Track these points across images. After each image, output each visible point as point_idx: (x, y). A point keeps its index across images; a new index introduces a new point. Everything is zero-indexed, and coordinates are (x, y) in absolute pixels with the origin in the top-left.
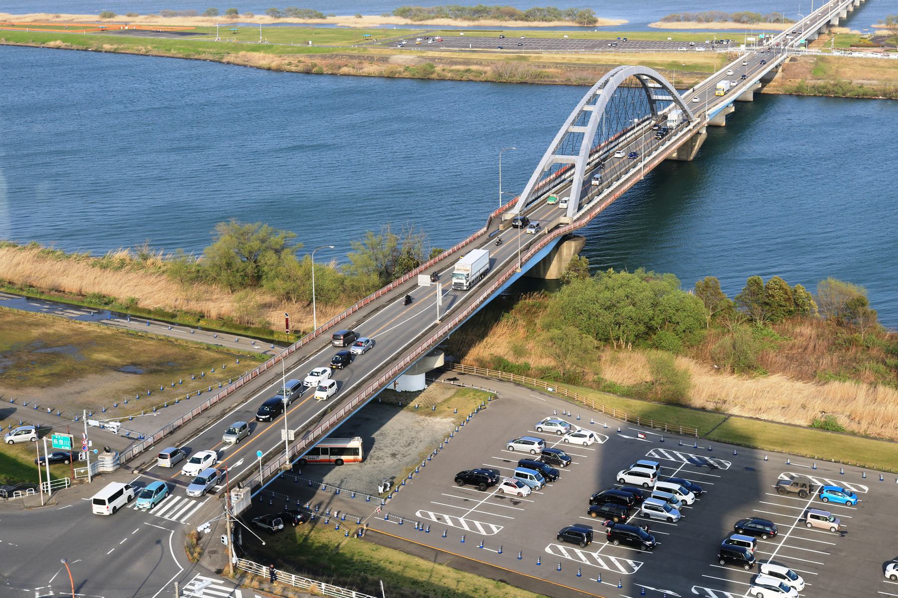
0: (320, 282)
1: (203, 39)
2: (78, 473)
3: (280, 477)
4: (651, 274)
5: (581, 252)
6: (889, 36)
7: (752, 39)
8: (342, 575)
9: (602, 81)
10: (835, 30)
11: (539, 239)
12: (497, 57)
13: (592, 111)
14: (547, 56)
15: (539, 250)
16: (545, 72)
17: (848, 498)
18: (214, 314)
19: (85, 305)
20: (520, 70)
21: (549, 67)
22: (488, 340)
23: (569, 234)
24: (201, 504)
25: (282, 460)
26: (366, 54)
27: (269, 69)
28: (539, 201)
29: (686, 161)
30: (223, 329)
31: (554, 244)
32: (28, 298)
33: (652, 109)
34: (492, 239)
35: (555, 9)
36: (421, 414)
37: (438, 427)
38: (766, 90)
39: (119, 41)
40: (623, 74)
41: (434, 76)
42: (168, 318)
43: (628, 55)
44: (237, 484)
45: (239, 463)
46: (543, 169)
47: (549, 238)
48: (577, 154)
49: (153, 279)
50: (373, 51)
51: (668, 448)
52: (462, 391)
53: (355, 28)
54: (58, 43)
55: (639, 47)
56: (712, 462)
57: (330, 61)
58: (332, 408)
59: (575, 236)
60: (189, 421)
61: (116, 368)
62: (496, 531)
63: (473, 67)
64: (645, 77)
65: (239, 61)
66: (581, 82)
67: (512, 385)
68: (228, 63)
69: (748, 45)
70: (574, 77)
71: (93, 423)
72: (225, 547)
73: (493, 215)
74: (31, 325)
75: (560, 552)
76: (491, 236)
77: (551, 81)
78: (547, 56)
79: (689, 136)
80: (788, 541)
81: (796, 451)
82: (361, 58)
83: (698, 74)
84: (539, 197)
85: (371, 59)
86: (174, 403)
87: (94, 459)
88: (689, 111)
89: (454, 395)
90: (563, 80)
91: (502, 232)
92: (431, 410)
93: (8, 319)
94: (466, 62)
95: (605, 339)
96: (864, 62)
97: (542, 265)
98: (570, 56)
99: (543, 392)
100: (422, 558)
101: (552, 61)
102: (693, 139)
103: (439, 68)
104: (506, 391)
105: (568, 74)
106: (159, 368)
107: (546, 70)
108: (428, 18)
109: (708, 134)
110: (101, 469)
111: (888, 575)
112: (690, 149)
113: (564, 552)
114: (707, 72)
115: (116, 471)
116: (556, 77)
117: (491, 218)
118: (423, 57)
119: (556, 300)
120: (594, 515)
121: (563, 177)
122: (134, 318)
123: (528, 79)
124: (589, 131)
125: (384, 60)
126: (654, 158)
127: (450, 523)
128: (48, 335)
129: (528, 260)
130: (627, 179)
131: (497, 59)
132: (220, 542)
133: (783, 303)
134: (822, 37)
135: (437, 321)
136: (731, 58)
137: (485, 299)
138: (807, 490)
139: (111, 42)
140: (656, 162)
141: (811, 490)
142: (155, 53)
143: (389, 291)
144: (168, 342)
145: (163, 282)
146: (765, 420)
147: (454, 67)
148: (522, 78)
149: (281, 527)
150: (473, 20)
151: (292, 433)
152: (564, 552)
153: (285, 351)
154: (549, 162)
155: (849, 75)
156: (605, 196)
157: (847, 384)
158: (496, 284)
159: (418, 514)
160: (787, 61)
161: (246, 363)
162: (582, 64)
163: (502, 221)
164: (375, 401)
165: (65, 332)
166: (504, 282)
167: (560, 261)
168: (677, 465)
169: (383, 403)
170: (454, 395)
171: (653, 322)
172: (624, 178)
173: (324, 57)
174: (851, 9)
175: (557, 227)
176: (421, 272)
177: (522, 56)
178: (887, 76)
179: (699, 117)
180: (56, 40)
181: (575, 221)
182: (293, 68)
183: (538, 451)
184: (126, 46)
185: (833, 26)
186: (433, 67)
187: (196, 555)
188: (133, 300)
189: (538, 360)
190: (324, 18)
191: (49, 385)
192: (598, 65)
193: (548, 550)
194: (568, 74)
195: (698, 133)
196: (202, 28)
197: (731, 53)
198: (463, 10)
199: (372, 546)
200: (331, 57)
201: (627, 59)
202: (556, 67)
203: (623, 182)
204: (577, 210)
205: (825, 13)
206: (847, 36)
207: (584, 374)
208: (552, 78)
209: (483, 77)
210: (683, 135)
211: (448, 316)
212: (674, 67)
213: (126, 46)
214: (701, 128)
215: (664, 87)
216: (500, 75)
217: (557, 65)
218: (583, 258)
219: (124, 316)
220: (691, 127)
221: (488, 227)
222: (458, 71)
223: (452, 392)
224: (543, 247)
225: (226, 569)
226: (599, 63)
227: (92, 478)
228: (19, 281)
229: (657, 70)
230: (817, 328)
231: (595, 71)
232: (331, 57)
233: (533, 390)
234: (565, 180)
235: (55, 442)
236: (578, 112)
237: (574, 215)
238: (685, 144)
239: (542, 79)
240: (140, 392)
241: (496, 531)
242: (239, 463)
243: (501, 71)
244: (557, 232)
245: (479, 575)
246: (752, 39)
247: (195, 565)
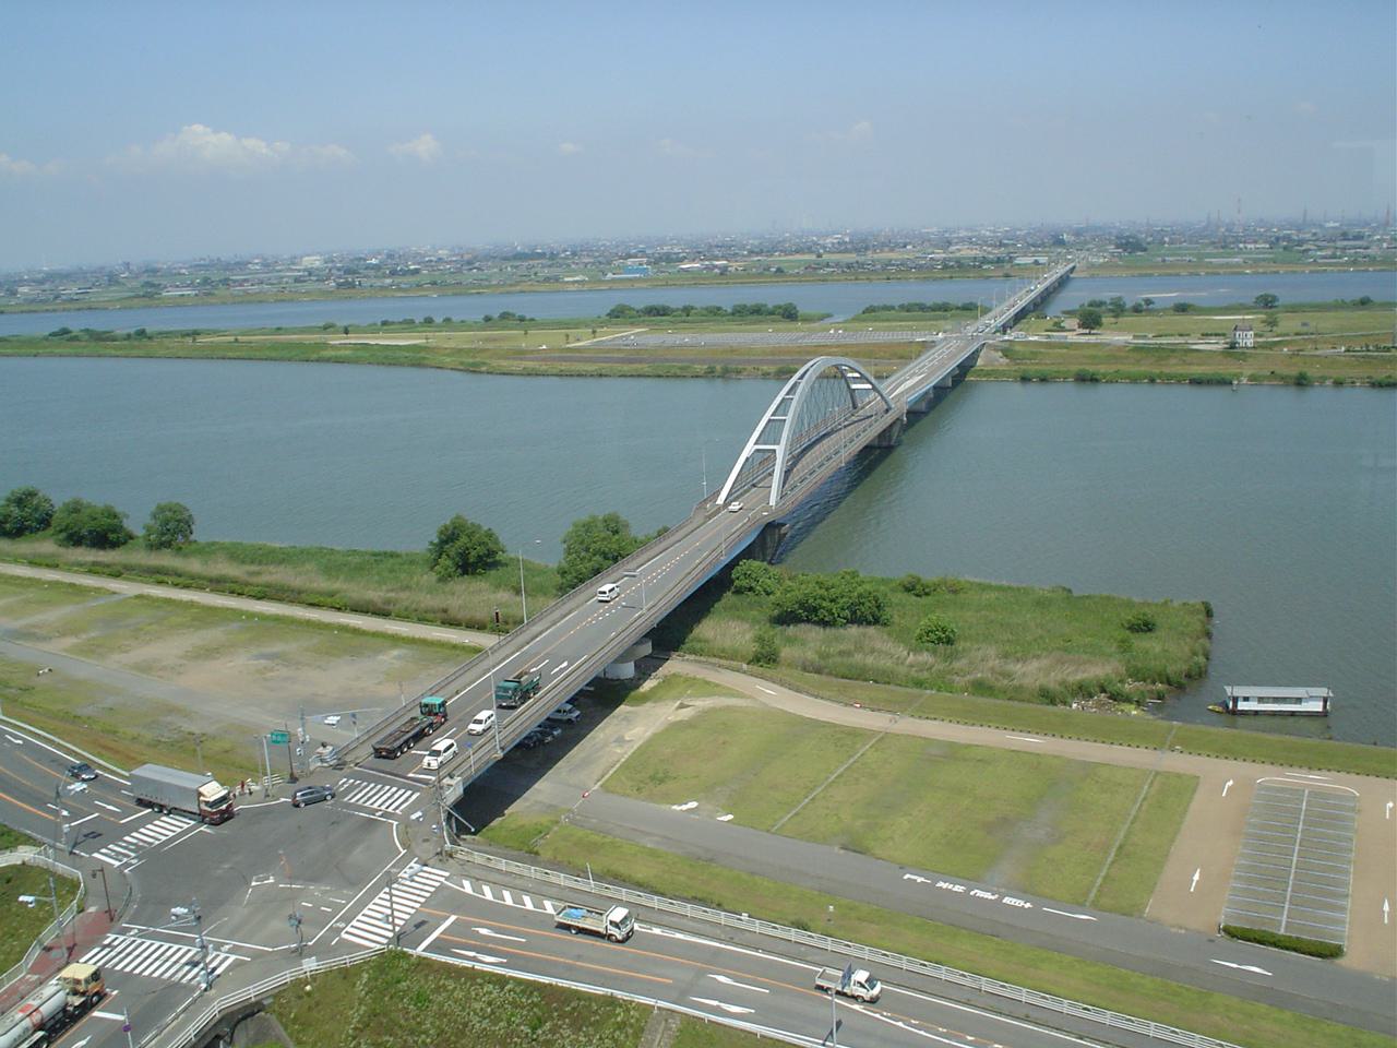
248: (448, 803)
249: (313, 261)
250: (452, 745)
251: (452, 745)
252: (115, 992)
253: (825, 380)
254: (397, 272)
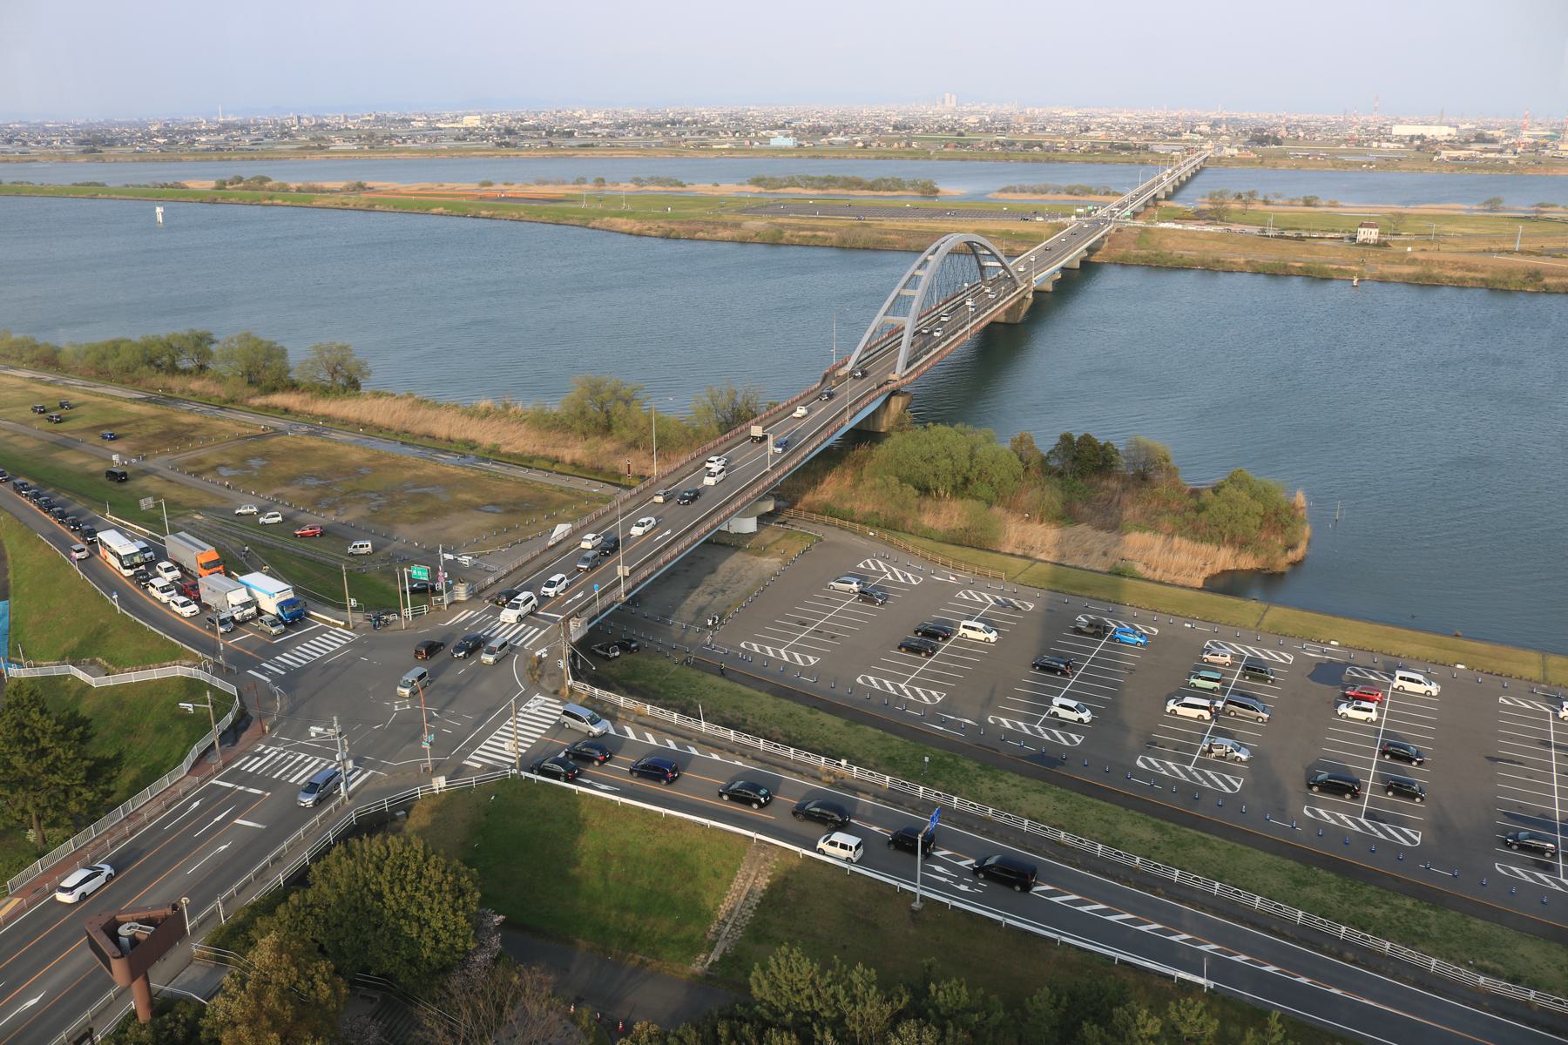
0: (660, 431)
1: (572, 206)
2: (436, 602)
3: (618, 608)
5: (905, 408)
6: (1211, 210)
7: (1080, 210)
8: (670, 698)
9: (933, 247)
10: (1161, 203)
14: (889, 223)
17: (1138, 639)
18: (568, 459)
19: (453, 449)
21: (890, 234)
22: (820, 488)
24: (543, 632)
25: (618, 594)
26: (720, 220)
27: (630, 234)
30: (575, 473)
31: (882, 399)
32: (403, 443)
33: (982, 275)
35: (899, 180)
36: (752, 554)
37: (766, 566)
38: (1094, 259)
39: (495, 208)
40: (954, 240)
41: (783, 241)
42: (526, 461)
44: (574, 615)
45: (579, 595)
48: (907, 316)
49: (514, 427)
50: (727, 217)
51: (978, 590)
52: (789, 535)
53: (713, 196)
54: (441, 209)
55: (977, 216)
56: (1016, 603)
57: (687, 227)
58: (667, 547)
60: (536, 556)
61: (477, 507)
62: (813, 662)
63: (820, 233)
65: (603, 226)
67: (836, 529)
68: (594, 228)
69: (1078, 215)
70: (913, 243)
71: (449, 557)
72: (562, 671)
74: (403, 467)
75: (870, 683)
78: (889, 223)
80: (1081, 677)
81: (1094, 595)
82: (716, 224)
85: (725, 225)
86: (528, 540)
87: (449, 588)
89: (782, 538)
91: (834, 387)
92: (761, 551)
93: (384, 462)
94: (814, 229)
95: (925, 490)
96: (1185, 234)
98: (910, 224)
99: (864, 536)
100: (744, 685)
102: (1020, 303)
103: (788, 233)
104: (832, 535)
105: (908, 240)
106: (516, 508)
108: (781, 187)
110: (456, 598)
111: (1168, 710)
113: (874, 682)
115: (469, 600)
118: (774, 224)
119: (882, 451)
120: (903, 650)
122: (496, 461)
123: (870, 245)
124: (918, 294)
125: (737, 225)
127: (771, 654)
128: (419, 476)
132: (556, 666)
133: (1092, 458)
134: (1149, 209)
135: (768, 469)
136: (1061, 227)
137: (814, 449)
138: (1102, 631)
139: (488, 208)
140: (983, 324)
141: (1105, 631)
142: (527, 218)
143: (726, 440)
144: (524, 483)
145: (523, 429)
146: (1068, 566)
147: (801, 233)
149: (617, 654)
150: (823, 189)
151: (627, 569)
152: (874, 682)
153: (626, 494)
155: (1171, 245)
157: (1147, 534)
159: (742, 645)
160: (1113, 232)
161: (594, 505)
164: (707, 542)
165: (433, 474)
168: (984, 605)
169: (716, 543)
170: (782, 538)
171: (970, 473)
173: (682, 223)
174: (1177, 183)
176: (756, 424)
178: (1206, 248)
180: (439, 207)
182: (653, 233)
183: (856, 590)
184: (501, 212)
185: (1160, 199)
186: (781, 232)
187: (536, 677)
188: (495, 445)
189: (865, 505)
190: (684, 186)
191: (417, 521)
193: (859, 680)
194: (908, 240)
195: (1024, 298)
196: (571, 195)
197: (1061, 223)
198: (812, 179)
199: (700, 673)
200: (689, 222)
205: (1152, 186)
206: (1172, 209)
207: (904, 520)
209: (828, 243)
211: (778, 464)
212: (1007, 235)
213: (501, 212)
215: (993, 254)
216: (844, 241)
217: (897, 232)
219: (487, 460)
220: (1019, 290)
222: (805, 236)
223: (780, 535)
224: (871, 402)
225: (562, 691)
227: (448, 606)
228: (396, 428)
229: (988, 238)
230: (1123, 482)
232: (689, 222)
233: (855, 533)
235: (414, 572)
238: (1012, 307)
240: (499, 530)
241: (813, 662)
242: (579, 595)
244: (885, 387)
245: (795, 702)
246: (1080, 210)
247: (535, 686)
248: (573, 641)
249: (472, 121)
250: (531, 598)
251: (531, 598)
252: (268, 794)
253: (956, 257)
254: (556, 136)
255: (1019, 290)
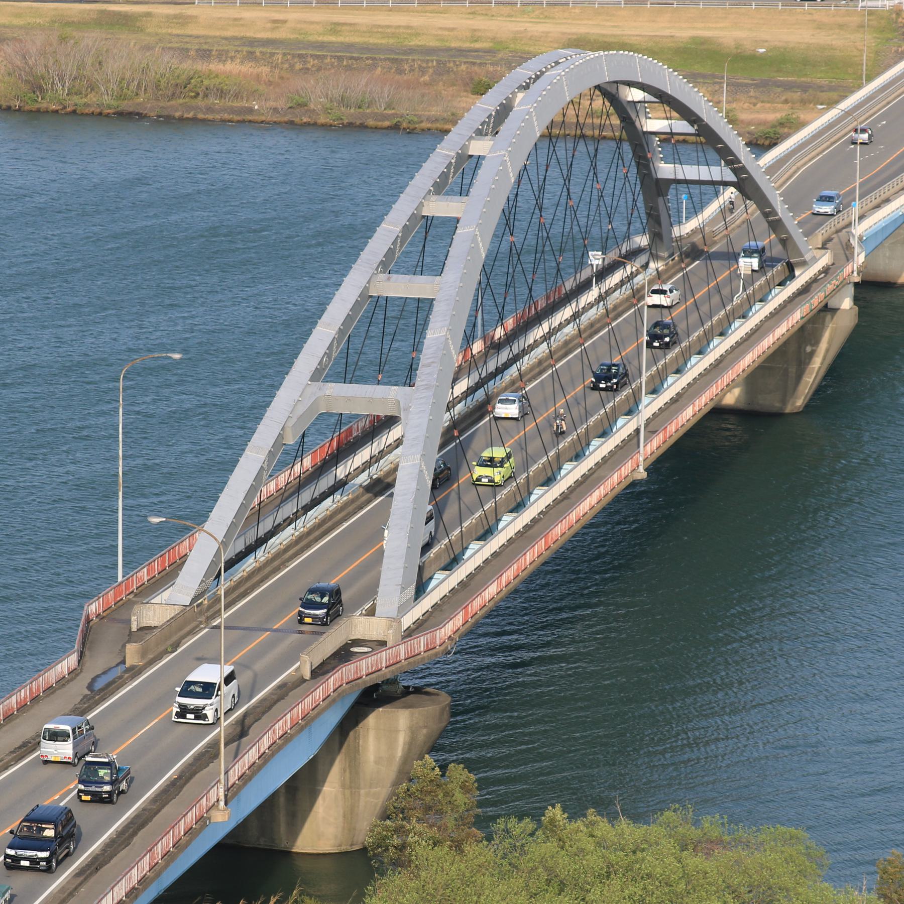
4: (712, 825)
11: (281, 698)
12: (18, 15)
13: (458, 220)
15: (286, 738)
16: (210, 75)
20: (113, 67)
21: (222, 56)
23: (388, 682)
28: (261, 555)
29: (777, 416)
31: (333, 718)
34: (103, 699)
43: (523, 12)
46: (281, 436)
47: (319, 694)
59: (407, 691)
64: (636, 95)
66: (349, 114)
73: (94, 608)
76: (99, 685)
77: (232, 111)
79: (796, 317)
83: (789, 87)
84: (261, 542)
88: (791, 222)
90: (281, 104)
91: (135, 672)
97: (282, 800)
101: (229, 33)
107: (212, 67)
109: (861, 314)
112: (793, 370)
114: (824, 82)
116: (254, 94)
117: (88, 620)
121: (341, 471)
123: (143, 101)
126: (677, 401)
129: (250, 778)
130: (585, 477)
131: (17, 22)
148: (121, 97)
154: (301, 409)
156: (511, 541)
158: (145, 865)
162: (349, 47)
163: (131, 633)
166: (169, 857)
167: (352, 784)
172: (571, 473)
175: (343, 655)
177: (119, 14)
179: (824, 247)
181: (410, 633)
192: (411, 51)
195: (827, 310)
201: (520, 27)
202: (250, 56)
203: (571, 490)
204: (412, 590)
208: (237, 96)
210: (772, 315)
214: (838, 289)
216: (37, 87)
218: (458, 773)
220: (802, 277)
221: (81, 655)
226: (415, 42)
231: (400, 72)
234: (340, 485)
236: (404, 221)
237: (403, 609)
239: (200, 102)
243: (40, 70)
255: (802, 277)
